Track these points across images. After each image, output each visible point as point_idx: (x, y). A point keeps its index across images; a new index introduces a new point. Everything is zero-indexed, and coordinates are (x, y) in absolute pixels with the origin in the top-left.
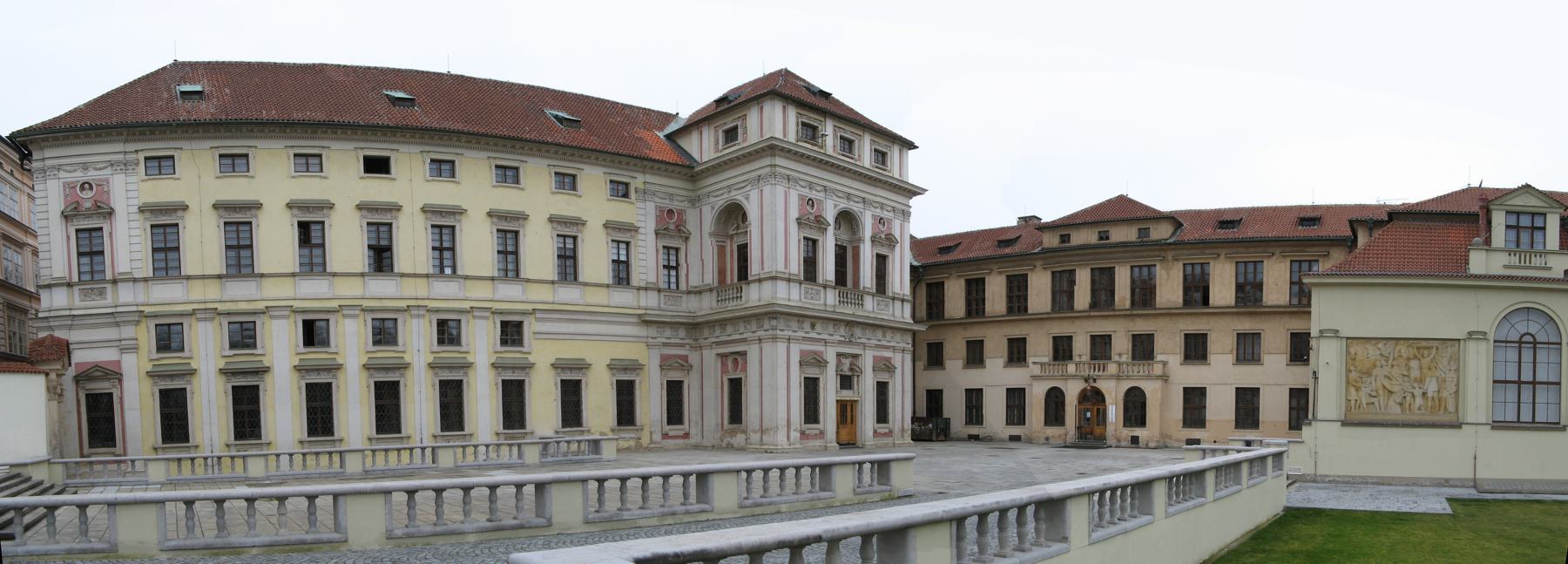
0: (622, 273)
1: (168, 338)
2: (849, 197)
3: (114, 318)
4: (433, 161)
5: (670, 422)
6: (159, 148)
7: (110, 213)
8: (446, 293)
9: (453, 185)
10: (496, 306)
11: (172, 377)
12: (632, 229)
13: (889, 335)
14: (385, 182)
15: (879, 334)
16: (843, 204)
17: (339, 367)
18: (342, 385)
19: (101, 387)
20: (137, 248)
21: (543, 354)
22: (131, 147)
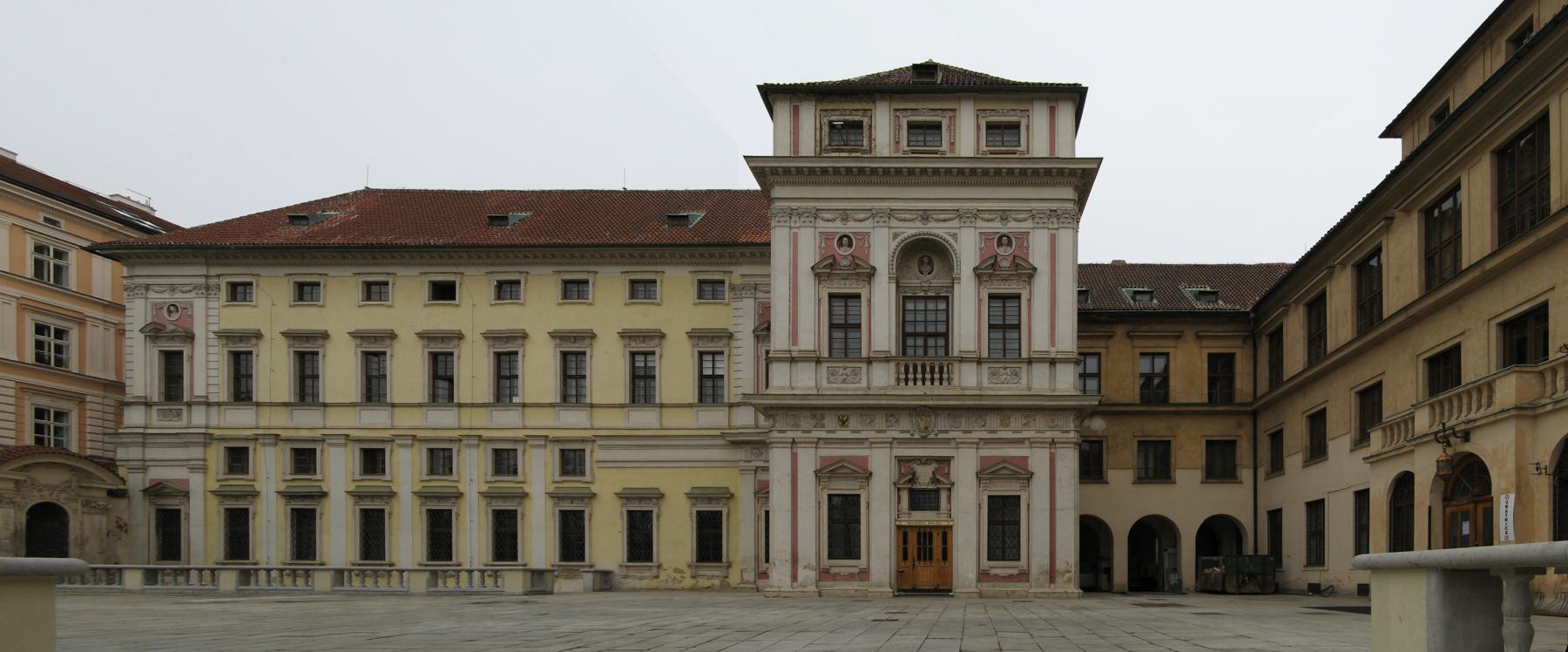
0: (709, 388)
1: (238, 458)
2: (1004, 216)
3: (181, 439)
4: (992, 297)
6: (238, 274)
8: (505, 422)
9: (516, 308)
11: (237, 497)
13: (1016, 422)
14: (449, 309)
15: (993, 421)
16: (911, 230)
17: (324, 495)
18: (395, 511)
19: (170, 503)
20: (214, 373)
21: (607, 484)
22: (214, 271)
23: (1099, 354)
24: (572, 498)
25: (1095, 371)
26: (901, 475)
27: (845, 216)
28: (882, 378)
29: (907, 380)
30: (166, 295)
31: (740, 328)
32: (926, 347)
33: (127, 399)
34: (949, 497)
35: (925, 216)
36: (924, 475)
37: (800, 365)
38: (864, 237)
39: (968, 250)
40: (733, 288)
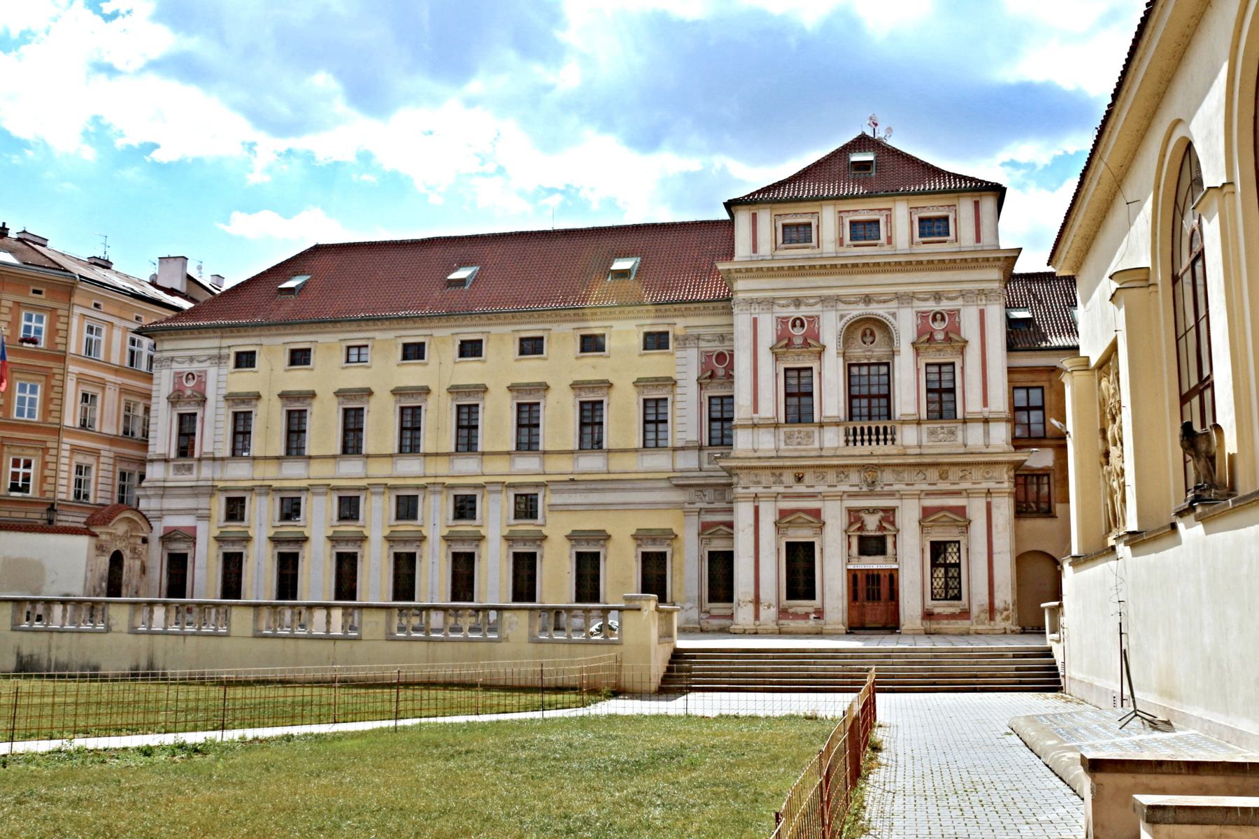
1: (235, 509)
3: (195, 491)
5: (810, 546)
7: (203, 401)
10: (508, 480)
12: (671, 382)
14: (418, 368)
15: (933, 474)
17: (306, 539)
19: (179, 548)
23: (1042, 388)
24: (289, 541)
25: (1040, 404)
26: (851, 524)
27: (798, 302)
28: (833, 439)
29: (855, 441)
30: (186, 365)
31: (684, 376)
32: (870, 407)
33: (150, 455)
34: (895, 543)
35: (867, 299)
36: (872, 523)
37: (762, 430)
38: (813, 319)
39: (906, 326)
40: (676, 338)
